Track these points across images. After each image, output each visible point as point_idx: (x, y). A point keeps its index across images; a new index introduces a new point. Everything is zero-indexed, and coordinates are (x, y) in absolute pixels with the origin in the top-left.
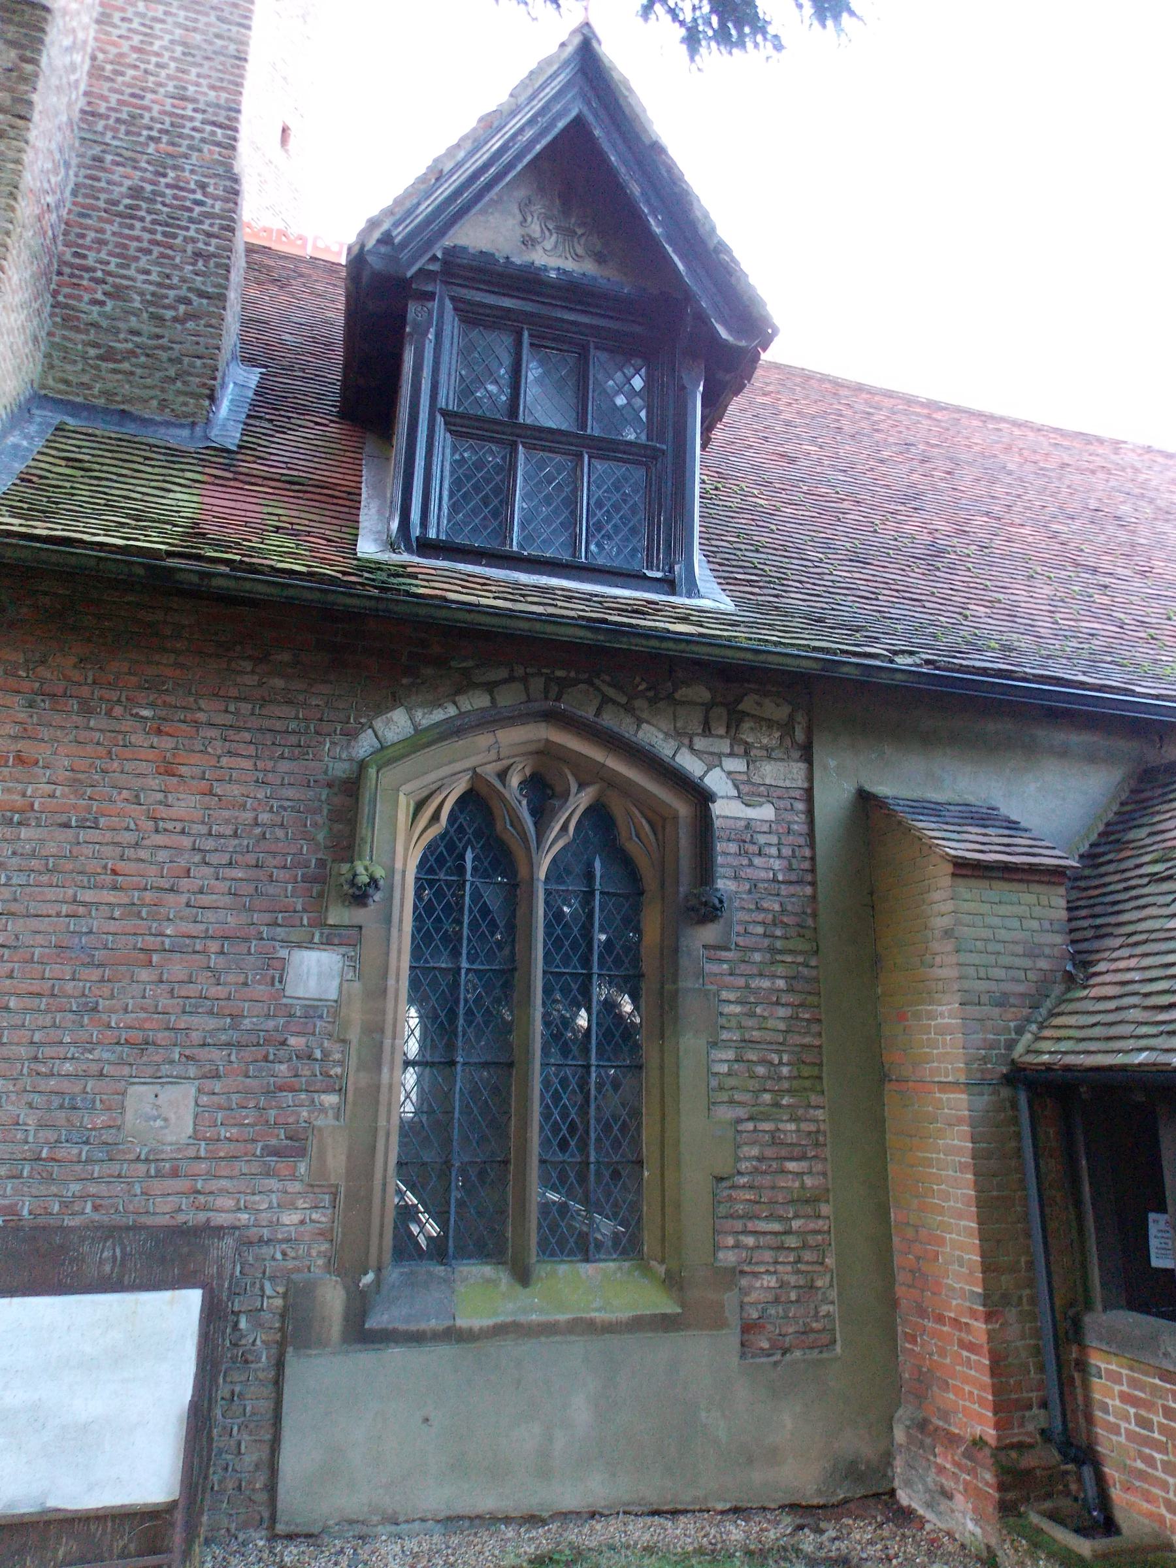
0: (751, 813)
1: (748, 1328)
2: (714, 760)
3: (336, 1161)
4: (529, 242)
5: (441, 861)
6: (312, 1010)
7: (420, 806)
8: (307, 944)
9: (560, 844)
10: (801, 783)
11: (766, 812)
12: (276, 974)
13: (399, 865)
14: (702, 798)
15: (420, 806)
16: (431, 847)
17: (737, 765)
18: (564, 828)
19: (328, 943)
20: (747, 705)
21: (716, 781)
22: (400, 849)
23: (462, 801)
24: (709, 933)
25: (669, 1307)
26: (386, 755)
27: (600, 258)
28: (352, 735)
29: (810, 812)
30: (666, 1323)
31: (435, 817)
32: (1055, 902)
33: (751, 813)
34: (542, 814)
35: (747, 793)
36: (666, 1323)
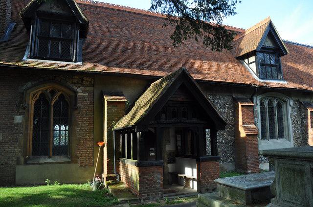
0: (84, 95)
1: (81, 163)
2: (78, 87)
3: (22, 143)
4: (52, 8)
5: (57, 103)
6: (18, 124)
7: (34, 95)
8: (17, 115)
9: (55, 100)
10: (93, 90)
11: (87, 94)
12: (13, 119)
13: (30, 104)
14: (76, 92)
15: (34, 95)
16: (36, 101)
17: (82, 88)
18: (56, 98)
19: (20, 115)
20: (84, 78)
21: (79, 90)
22: (30, 102)
23: (41, 94)
24: (76, 112)
25: (70, 161)
26: (28, 89)
27: (63, 10)
28: (23, 86)
29: (94, 94)
30: (69, 163)
31: (36, 97)
32: (255, 63)
33: (84, 95)
34: (53, 95)
35: (84, 92)
36: (69, 163)
